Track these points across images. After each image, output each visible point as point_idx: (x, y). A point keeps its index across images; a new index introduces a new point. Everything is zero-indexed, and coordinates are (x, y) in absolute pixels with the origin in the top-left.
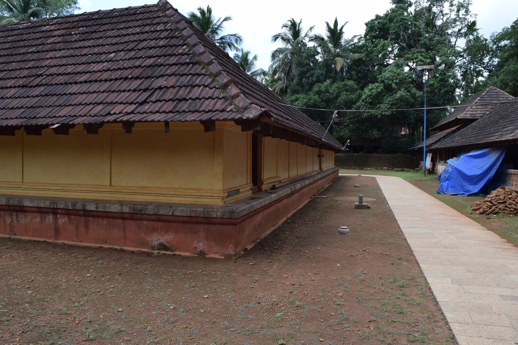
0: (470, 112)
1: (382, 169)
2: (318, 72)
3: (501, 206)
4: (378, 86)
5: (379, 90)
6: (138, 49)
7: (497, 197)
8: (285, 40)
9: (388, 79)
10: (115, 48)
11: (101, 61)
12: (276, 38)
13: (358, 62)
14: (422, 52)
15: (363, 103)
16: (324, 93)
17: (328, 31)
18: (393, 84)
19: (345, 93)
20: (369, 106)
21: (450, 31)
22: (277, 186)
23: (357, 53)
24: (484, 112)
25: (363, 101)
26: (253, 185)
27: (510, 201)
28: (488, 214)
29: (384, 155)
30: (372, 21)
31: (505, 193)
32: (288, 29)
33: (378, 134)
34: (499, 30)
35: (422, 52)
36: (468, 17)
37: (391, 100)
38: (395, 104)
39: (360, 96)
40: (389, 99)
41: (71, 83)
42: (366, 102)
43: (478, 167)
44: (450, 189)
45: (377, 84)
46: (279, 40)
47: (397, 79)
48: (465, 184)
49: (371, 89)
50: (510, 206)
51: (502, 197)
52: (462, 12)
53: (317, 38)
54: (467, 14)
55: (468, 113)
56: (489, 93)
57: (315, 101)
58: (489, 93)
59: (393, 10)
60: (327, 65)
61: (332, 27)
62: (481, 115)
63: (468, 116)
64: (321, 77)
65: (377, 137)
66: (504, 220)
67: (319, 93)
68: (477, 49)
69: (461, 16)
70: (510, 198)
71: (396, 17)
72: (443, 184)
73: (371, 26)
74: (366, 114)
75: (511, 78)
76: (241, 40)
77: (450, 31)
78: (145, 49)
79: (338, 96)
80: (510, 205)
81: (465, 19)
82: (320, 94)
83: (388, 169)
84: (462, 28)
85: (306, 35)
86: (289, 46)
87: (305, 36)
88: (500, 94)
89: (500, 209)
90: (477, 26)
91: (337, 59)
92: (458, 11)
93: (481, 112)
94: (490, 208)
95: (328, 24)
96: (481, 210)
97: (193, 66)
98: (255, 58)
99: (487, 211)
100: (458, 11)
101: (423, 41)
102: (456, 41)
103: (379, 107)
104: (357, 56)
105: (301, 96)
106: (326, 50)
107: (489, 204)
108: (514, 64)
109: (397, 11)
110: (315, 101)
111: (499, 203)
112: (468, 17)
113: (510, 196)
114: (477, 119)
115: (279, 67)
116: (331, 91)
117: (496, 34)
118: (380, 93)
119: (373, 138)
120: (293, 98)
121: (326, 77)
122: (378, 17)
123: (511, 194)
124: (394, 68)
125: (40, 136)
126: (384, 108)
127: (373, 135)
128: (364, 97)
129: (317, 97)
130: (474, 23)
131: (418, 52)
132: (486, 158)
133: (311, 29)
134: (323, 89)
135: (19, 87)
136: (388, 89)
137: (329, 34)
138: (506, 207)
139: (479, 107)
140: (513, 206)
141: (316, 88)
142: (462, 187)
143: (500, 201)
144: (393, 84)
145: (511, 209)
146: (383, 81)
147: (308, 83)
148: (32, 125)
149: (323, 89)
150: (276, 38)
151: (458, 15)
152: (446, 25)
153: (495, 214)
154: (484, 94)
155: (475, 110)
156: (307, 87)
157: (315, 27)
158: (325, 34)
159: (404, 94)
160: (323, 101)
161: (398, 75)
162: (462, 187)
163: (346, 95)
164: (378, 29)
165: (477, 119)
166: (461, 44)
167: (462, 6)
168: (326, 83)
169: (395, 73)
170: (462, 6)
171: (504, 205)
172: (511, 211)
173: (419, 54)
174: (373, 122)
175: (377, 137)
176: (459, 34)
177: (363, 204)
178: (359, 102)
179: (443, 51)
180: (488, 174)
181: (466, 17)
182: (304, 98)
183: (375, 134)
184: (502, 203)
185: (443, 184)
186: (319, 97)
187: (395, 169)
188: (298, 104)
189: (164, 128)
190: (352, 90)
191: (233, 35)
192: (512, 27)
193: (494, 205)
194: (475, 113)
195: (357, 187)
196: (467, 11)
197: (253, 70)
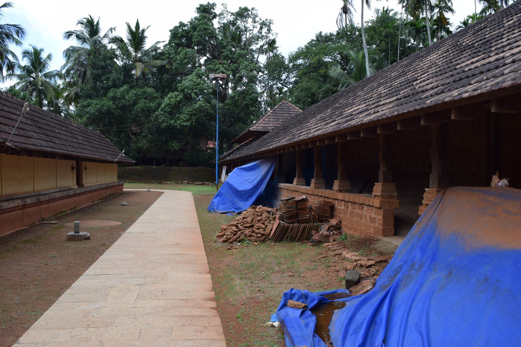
0: (262, 125)
1: (182, 183)
2: (114, 75)
3: (247, 232)
4: (178, 95)
5: (178, 99)
7: (245, 220)
8: (80, 39)
9: (187, 87)
13: (162, 69)
14: (223, 64)
15: (162, 113)
16: (120, 99)
17: (130, 34)
18: (193, 94)
19: (143, 100)
20: (167, 116)
21: (254, 47)
23: (160, 60)
24: (276, 125)
25: (162, 110)
27: (259, 224)
28: (232, 242)
29: (184, 168)
30: (176, 27)
31: (253, 214)
32: (84, 26)
33: (177, 146)
34: (294, 50)
35: (223, 64)
36: (270, 35)
37: (191, 110)
38: (195, 115)
39: (159, 105)
40: (188, 109)
42: (165, 112)
43: (249, 181)
44: (220, 206)
45: (176, 93)
46: (73, 38)
47: (196, 88)
48: (236, 200)
49: (171, 98)
50: (257, 231)
51: (249, 219)
52: (265, 30)
53: (117, 40)
54: (269, 33)
55: (260, 125)
56: (282, 107)
57: (109, 109)
58: (282, 107)
59: (196, 19)
60: (127, 69)
61: (134, 29)
62: (272, 128)
63: (260, 129)
64: (117, 82)
65: (177, 149)
66: (245, 250)
67: (114, 99)
68: (276, 66)
69: (263, 34)
70: (259, 221)
71: (199, 25)
72: (214, 200)
73: (175, 34)
74: (165, 125)
75: (304, 95)
76: (23, 32)
77: (254, 47)
79: (135, 103)
80: (258, 229)
81: (267, 37)
82: (116, 100)
83: (188, 183)
84: (263, 45)
85: (105, 36)
86: (87, 46)
87: (104, 37)
88: (291, 108)
89: (245, 235)
90: (277, 45)
91: (137, 63)
92: (261, 28)
93: (273, 125)
94: (234, 235)
95: (129, 27)
96: (225, 237)
98: (49, 57)
99: (230, 238)
100: (261, 28)
101: (226, 52)
102: (258, 57)
103: (178, 117)
104: (159, 62)
105: (94, 101)
106: (126, 53)
107: (234, 228)
108: (307, 82)
109: (200, 20)
110: (109, 107)
111: (246, 227)
112: (270, 35)
113: (259, 218)
114: (269, 132)
115: (72, 68)
116: (127, 97)
117: (294, 53)
118: (180, 102)
119: (173, 150)
120: (85, 103)
121: (124, 83)
122: (182, 25)
123: (261, 215)
124: (194, 77)
126: (183, 120)
127: (173, 146)
128: (163, 106)
129: (111, 103)
130: (274, 41)
131: (220, 63)
132: (257, 171)
133: (111, 30)
134: (119, 95)
136: (188, 99)
137: (130, 37)
138: (253, 232)
139: (271, 120)
140: (261, 231)
141: (111, 94)
142: (233, 203)
143: (248, 225)
144: (193, 94)
145: (259, 235)
146: (183, 91)
147: (103, 88)
149: (119, 95)
150: (69, 34)
151: (261, 33)
152: (250, 42)
153: (239, 242)
154: (276, 107)
155: (268, 122)
156: (102, 92)
157: (114, 25)
158: (125, 36)
159: (203, 105)
160: (118, 108)
161: (198, 84)
162: (233, 203)
163: (145, 102)
164: (181, 36)
165: (269, 132)
166: (262, 59)
167: (265, 25)
168: (122, 89)
169: (195, 82)
170: (265, 25)
171: (250, 230)
172: (258, 237)
173: (221, 66)
174: (173, 133)
175: (177, 149)
176: (261, 51)
177: (81, 233)
178: (158, 111)
179: (244, 65)
180: (259, 189)
181: (268, 35)
182: (96, 104)
183: (175, 145)
184: (250, 227)
185: (214, 200)
186: (114, 103)
187: (196, 183)
188: (90, 110)
190: (153, 99)
191: (14, 26)
192: (307, 47)
193: (240, 230)
194: (267, 125)
195: (125, 205)
196: (269, 30)
197: (47, 71)
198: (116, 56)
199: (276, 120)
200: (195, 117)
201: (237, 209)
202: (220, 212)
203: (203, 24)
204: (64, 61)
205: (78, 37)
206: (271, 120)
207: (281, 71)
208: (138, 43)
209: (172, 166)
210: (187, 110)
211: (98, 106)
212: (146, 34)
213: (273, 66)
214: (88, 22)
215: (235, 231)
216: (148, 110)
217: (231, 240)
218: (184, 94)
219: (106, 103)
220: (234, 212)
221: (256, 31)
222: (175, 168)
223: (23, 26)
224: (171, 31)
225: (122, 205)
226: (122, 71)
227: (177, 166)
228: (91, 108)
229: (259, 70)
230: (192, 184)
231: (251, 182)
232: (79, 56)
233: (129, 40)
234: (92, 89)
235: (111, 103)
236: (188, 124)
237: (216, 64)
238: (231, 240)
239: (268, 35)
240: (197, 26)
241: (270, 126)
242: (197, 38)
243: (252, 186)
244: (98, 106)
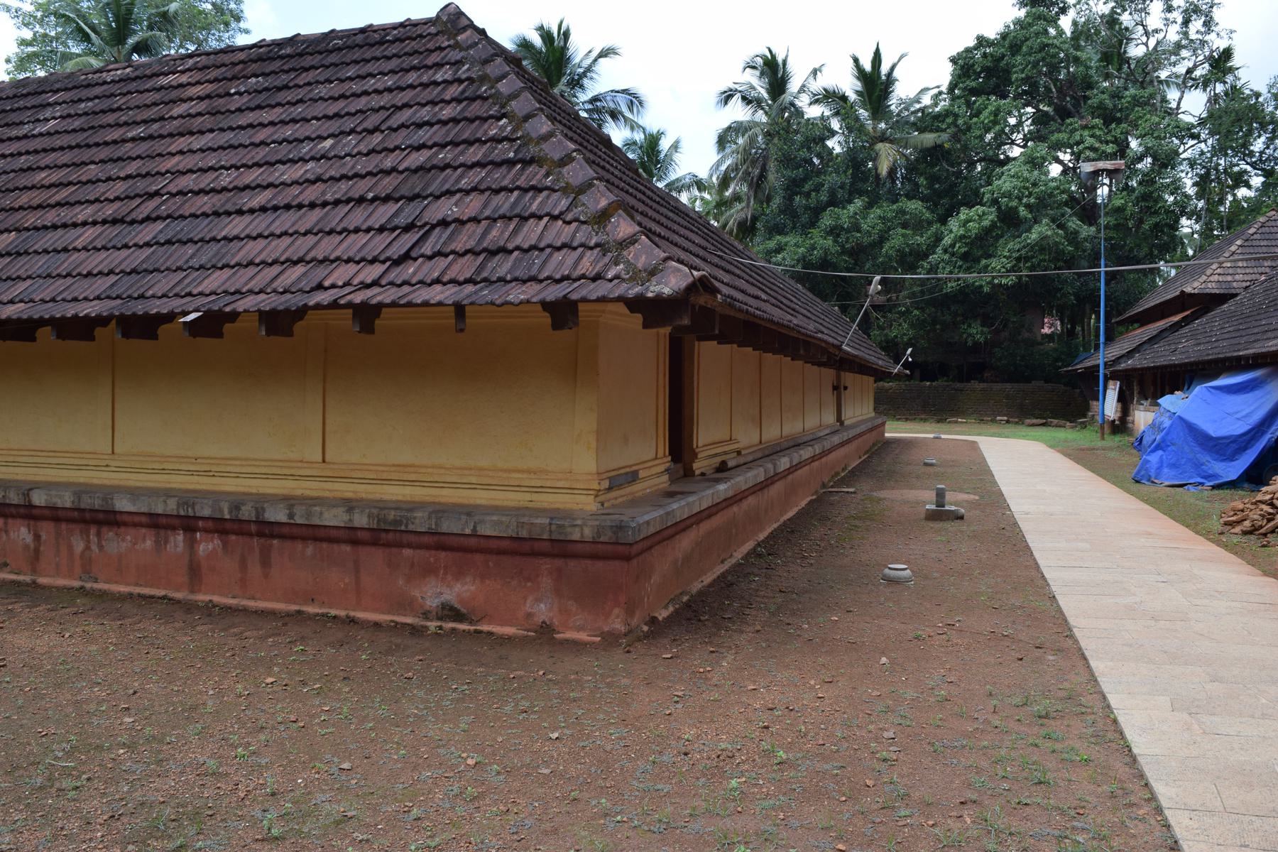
0: (1216, 278)
2: (831, 179)
4: (984, 214)
5: (986, 223)
6: (390, 128)
9: (1008, 195)
11: (301, 159)
13: (934, 154)
14: (1093, 127)
15: (946, 257)
16: (848, 231)
17: (858, 78)
18: (1021, 209)
19: (900, 231)
20: (960, 263)
23: (931, 131)
24: (1254, 277)
25: (945, 251)
28: (1265, 535)
29: (997, 386)
30: (968, 50)
32: (757, 73)
33: (982, 333)
35: (1093, 127)
36: (1211, 37)
37: (1017, 247)
38: (1027, 259)
39: (938, 239)
40: (1010, 246)
42: (953, 254)
43: (1239, 416)
44: (1166, 470)
45: (980, 209)
46: (736, 101)
48: (1205, 458)
49: (967, 221)
53: (832, 97)
55: (1212, 278)
59: (1018, 22)
60: (856, 161)
61: (868, 67)
62: (1245, 284)
63: (1212, 288)
67: (834, 231)
71: (1027, 40)
73: (964, 65)
76: (641, 103)
78: (408, 127)
79: (882, 239)
81: (1203, 43)
83: (1008, 422)
85: (803, 89)
86: (761, 117)
87: (799, 92)
90: (1236, 61)
91: (880, 146)
92: (1186, 22)
94: (1269, 520)
95: (856, 60)
96: (1247, 524)
98: (675, 146)
99: (1261, 527)
100: (1186, 22)
101: (1095, 98)
102: (1180, 99)
103: (986, 266)
104: (929, 138)
105: (791, 239)
106: (853, 125)
107: (1267, 508)
109: (1030, 25)
110: (826, 251)
114: (1236, 295)
115: (735, 168)
116: (865, 227)
118: (987, 231)
119: (970, 343)
120: (772, 244)
121: (854, 192)
126: (998, 270)
127: (970, 335)
128: (947, 241)
129: (830, 242)
130: (1227, 54)
131: (1084, 127)
132: (1258, 393)
133: (815, 72)
135: (104, 222)
136: (1010, 220)
137: (858, 85)
139: (1240, 264)
141: (827, 220)
142: (1198, 465)
144: (1021, 209)
147: (807, 208)
150: (727, 97)
154: (1252, 231)
155: (1231, 271)
156: (805, 218)
158: (849, 86)
159: (1049, 233)
160: (844, 252)
161: (1035, 185)
162: (1198, 465)
163: (903, 235)
164: (983, 71)
165: (1236, 295)
166: (1194, 105)
169: (1027, 180)
173: (1086, 133)
174: (971, 302)
177: (947, 508)
178: (934, 253)
179: (1148, 124)
180: (1264, 433)
181: (1207, 38)
183: (976, 332)
186: (835, 241)
188: (784, 259)
189: (454, 321)
190: (918, 225)
191: (624, 91)
194: (1229, 278)
195: (931, 465)
196: (1208, 24)
197: (673, 176)
198: (833, 133)
199: (1253, 263)
200: (1028, 264)
201: (1208, 477)
202: (1167, 483)
203: (1037, 34)
204: (714, 156)
205: (746, 100)
206: (1240, 264)
207: (1250, 132)
208: (880, 97)
209: (968, 381)
210: (1009, 247)
211: (802, 250)
212: (896, 74)
213: (1227, 120)
214: (765, 64)
215: (1270, 514)
216: (911, 254)
217: (1262, 531)
218: (999, 208)
219: (822, 242)
220: (1202, 484)
221: (1173, 35)
222: (976, 385)
223: (642, 91)
224: (953, 60)
225: (926, 464)
226: (848, 168)
227: (982, 380)
228: (784, 254)
229: (1188, 132)
230: (1017, 423)
231: (1245, 416)
232: (752, 140)
233: (857, 92)
234: (781, 212)
235: (829, 242)
236: (1009, 280)
237: (1073, 131)
238: (1262, 531)
239: (1207, 38)
240: (1023, 42)
241: (1238, 280)
242: (1022, 71)
243: (1247, 428)
244: (802, 250)
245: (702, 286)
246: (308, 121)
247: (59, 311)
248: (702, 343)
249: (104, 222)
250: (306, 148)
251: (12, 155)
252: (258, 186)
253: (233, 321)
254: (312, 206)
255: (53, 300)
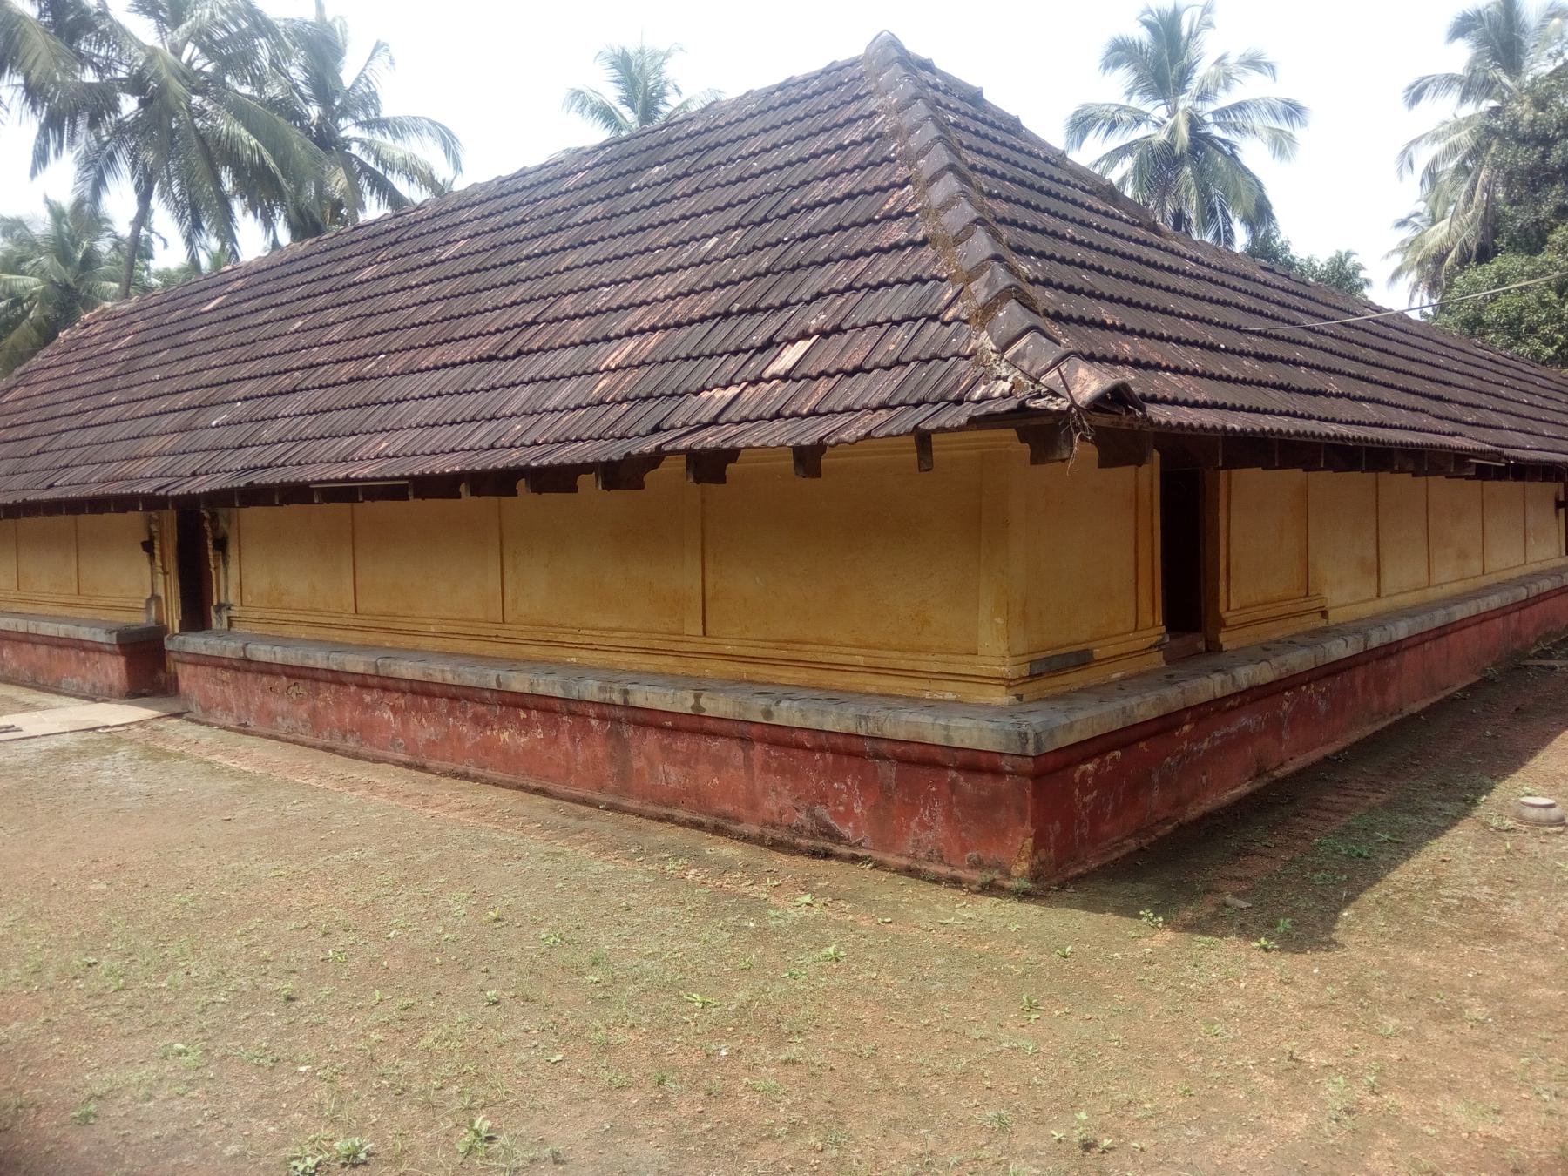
6: (778, 216)
10: (719, 221)
11: (680, 267)
12: (1416, 94)
22: (1099, 653)
26: (1168, 631)
41: (596, 341)
78: (798, 211)
97: (912, 252)
125: (639, 492)
135: (481, 360)
148: (641, 454)
150: (1416, 94)
189: (915, 455)
245: (1117, 398)
246: (699, 216)
247: (481, 462)
248: (1235, 472)
249: (481, 360)
250: (685, 255)
251: (417, 286)
252: (631, 305)
253: (734, 460)
254: (654, 329)
255: (492, 447)
